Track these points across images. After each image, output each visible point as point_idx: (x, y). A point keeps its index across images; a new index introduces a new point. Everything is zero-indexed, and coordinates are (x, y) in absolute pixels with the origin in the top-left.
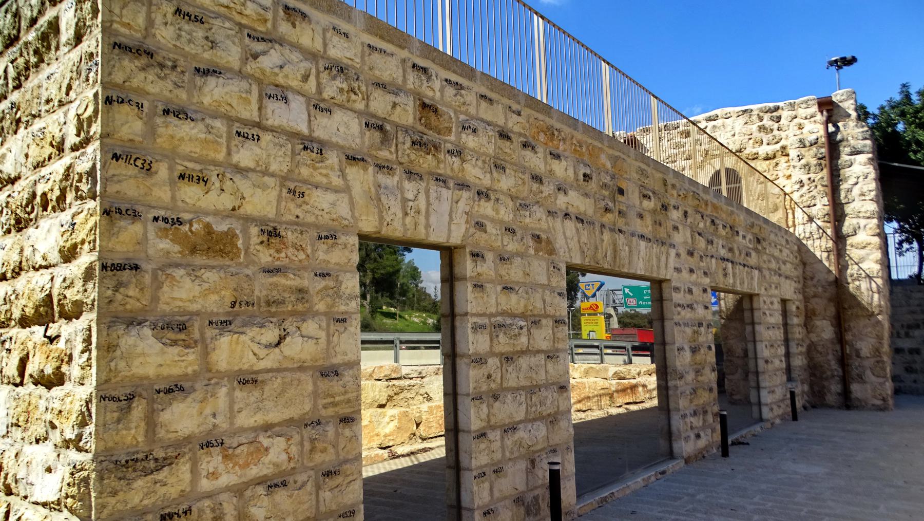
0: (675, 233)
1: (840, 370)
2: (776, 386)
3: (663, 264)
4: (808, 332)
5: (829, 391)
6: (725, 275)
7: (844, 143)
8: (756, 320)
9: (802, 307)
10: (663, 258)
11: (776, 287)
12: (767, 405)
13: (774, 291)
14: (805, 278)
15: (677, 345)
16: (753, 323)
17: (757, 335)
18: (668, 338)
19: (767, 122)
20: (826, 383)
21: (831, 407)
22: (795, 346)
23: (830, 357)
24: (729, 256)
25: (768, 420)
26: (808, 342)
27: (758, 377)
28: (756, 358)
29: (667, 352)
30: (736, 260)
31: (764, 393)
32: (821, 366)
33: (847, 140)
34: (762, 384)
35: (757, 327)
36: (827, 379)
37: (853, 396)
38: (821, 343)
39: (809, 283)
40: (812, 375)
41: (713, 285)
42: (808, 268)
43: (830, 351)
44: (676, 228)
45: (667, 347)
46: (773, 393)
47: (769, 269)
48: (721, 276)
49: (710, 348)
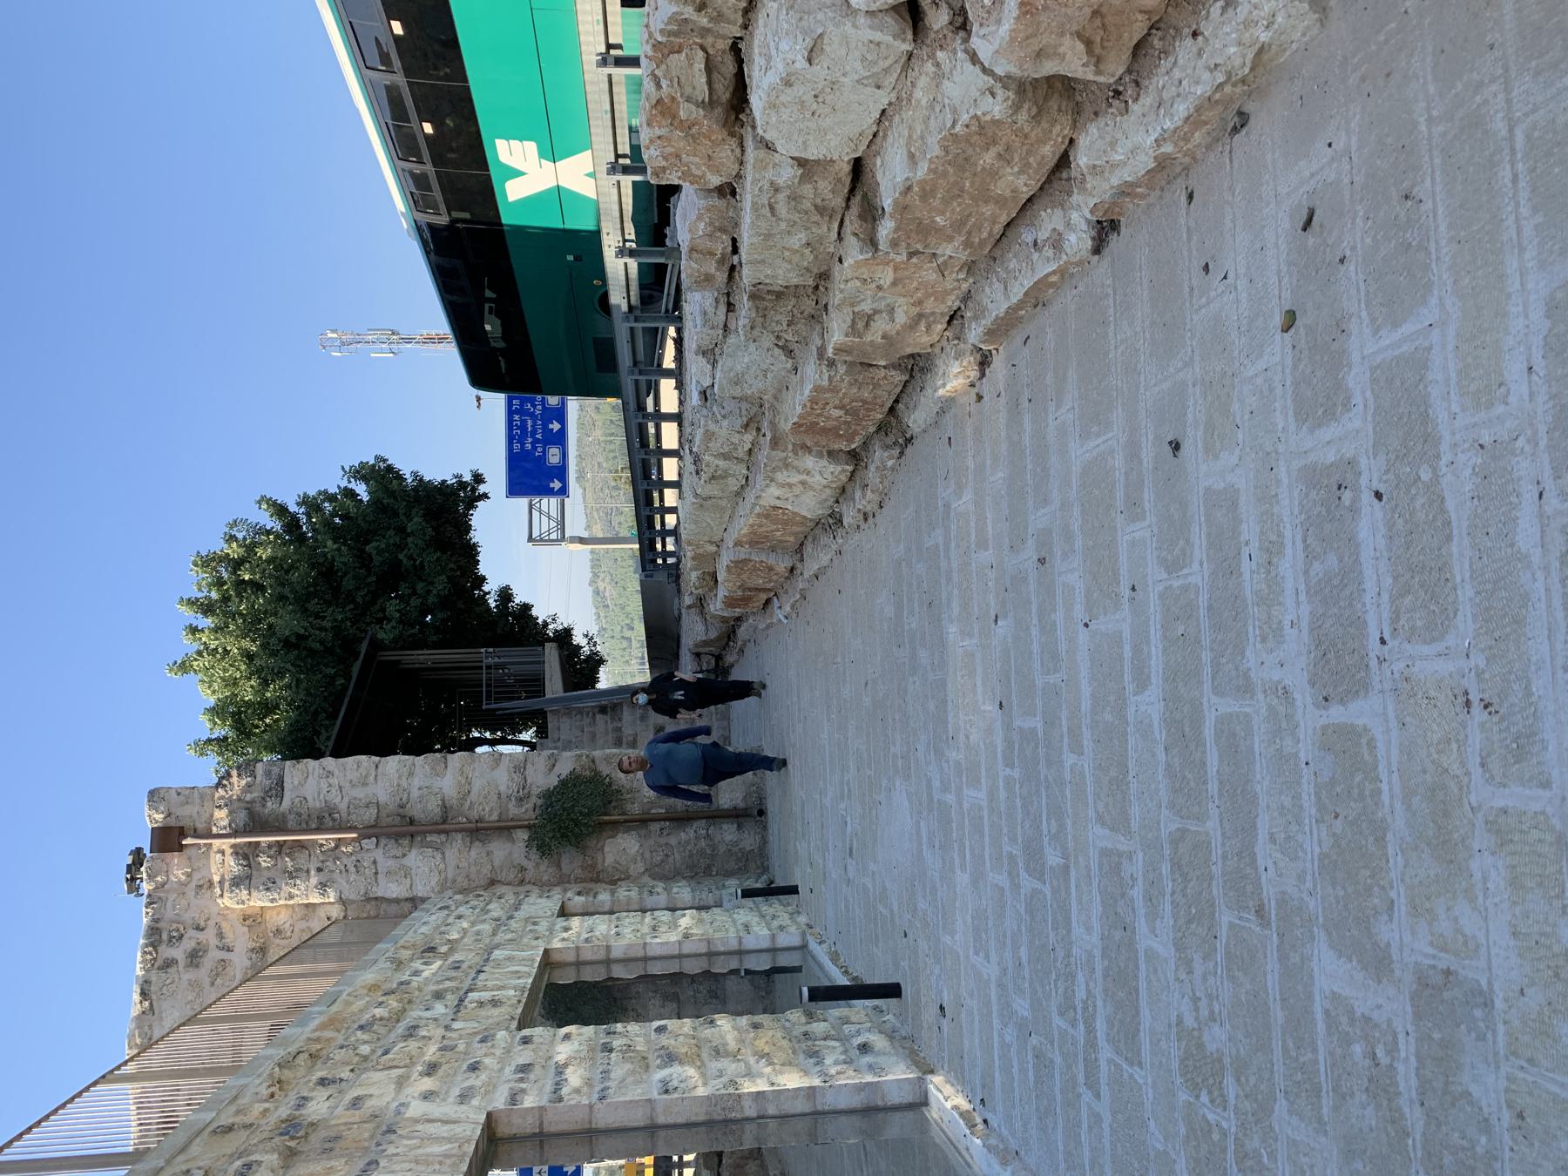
0: (370, 1105)
1: (696, 824)
2: (734, 921)
3: (444, 1130)
4: (628, 878)
5: (735, 844)
6: (495, 1003)
7: (258, 807)
8: (601, 955)
9: (577, 887)
10: (432, 1129)
11: (535, 924)
12: (773, 937)
13: (542, 927)
14: (522, 882)
15: (655, 1095)
16: (608, 962)
17: (632, 954)
18: (638, 1118)
19: (178, 953)
20: (722, 849)
21: (764, 841)
22: (655, 897)
23: (673, 841)
24: (451, 999)
25: (803, 934)
26: (646, 879)
27: (719, 954)
28: (680, 957)
29: (671, 1120)
30: (466, 986)
31: (750, 943)
32: (691, 856)
33: (252, 802)
34: (734, 945)
35: (616, 953)
36: (714, 847)
37: (742, 805)
38: (647, 855)
39: (529, 876)
40: (707, 872)
41: (514, 1024)
42: (502, 877)
43: (663, 841)
44: (356, 1103)
45: (661, 1120)
46: (744, 928)
47: (494, 934)
48: (495, 1012)
49: (660, 1030)
